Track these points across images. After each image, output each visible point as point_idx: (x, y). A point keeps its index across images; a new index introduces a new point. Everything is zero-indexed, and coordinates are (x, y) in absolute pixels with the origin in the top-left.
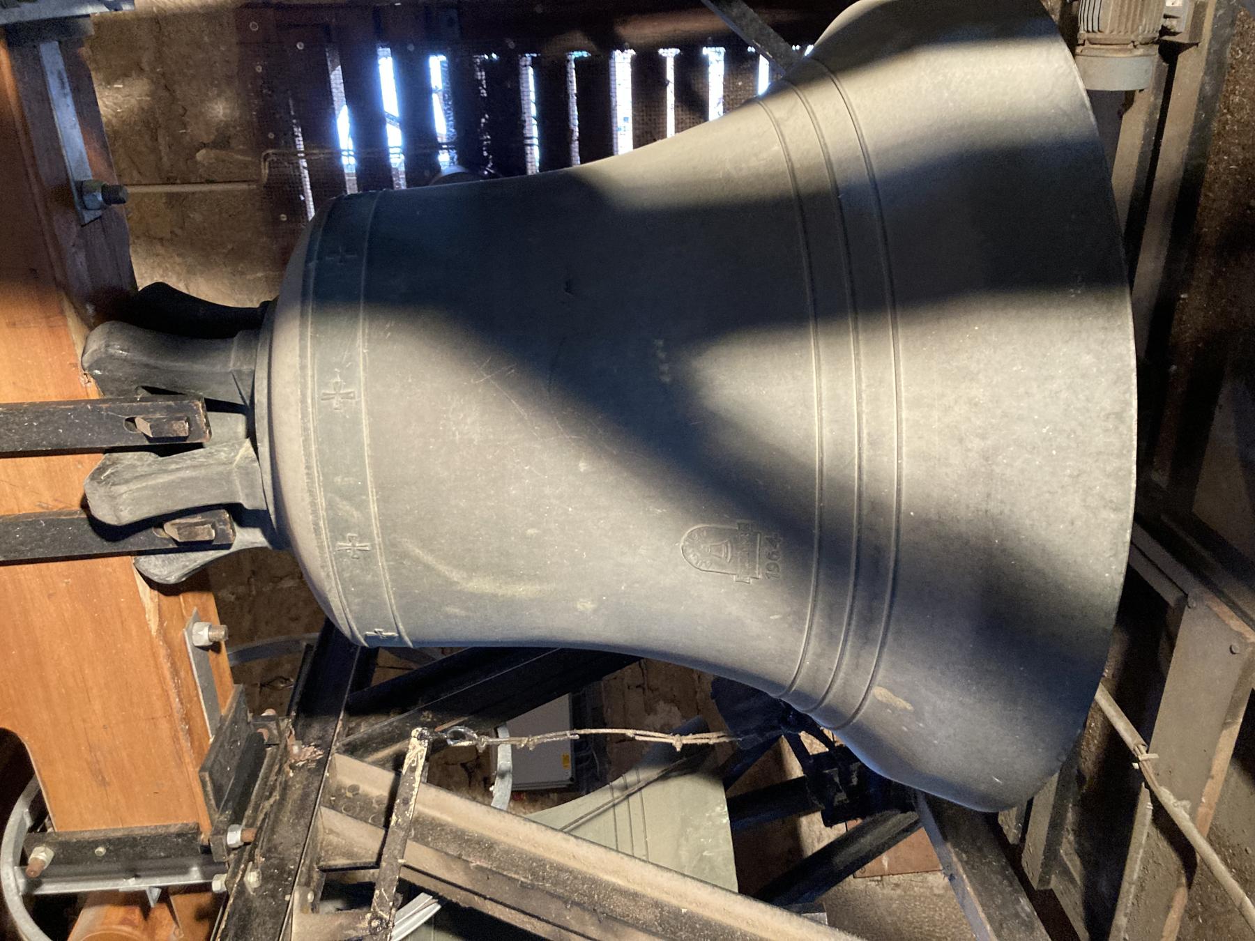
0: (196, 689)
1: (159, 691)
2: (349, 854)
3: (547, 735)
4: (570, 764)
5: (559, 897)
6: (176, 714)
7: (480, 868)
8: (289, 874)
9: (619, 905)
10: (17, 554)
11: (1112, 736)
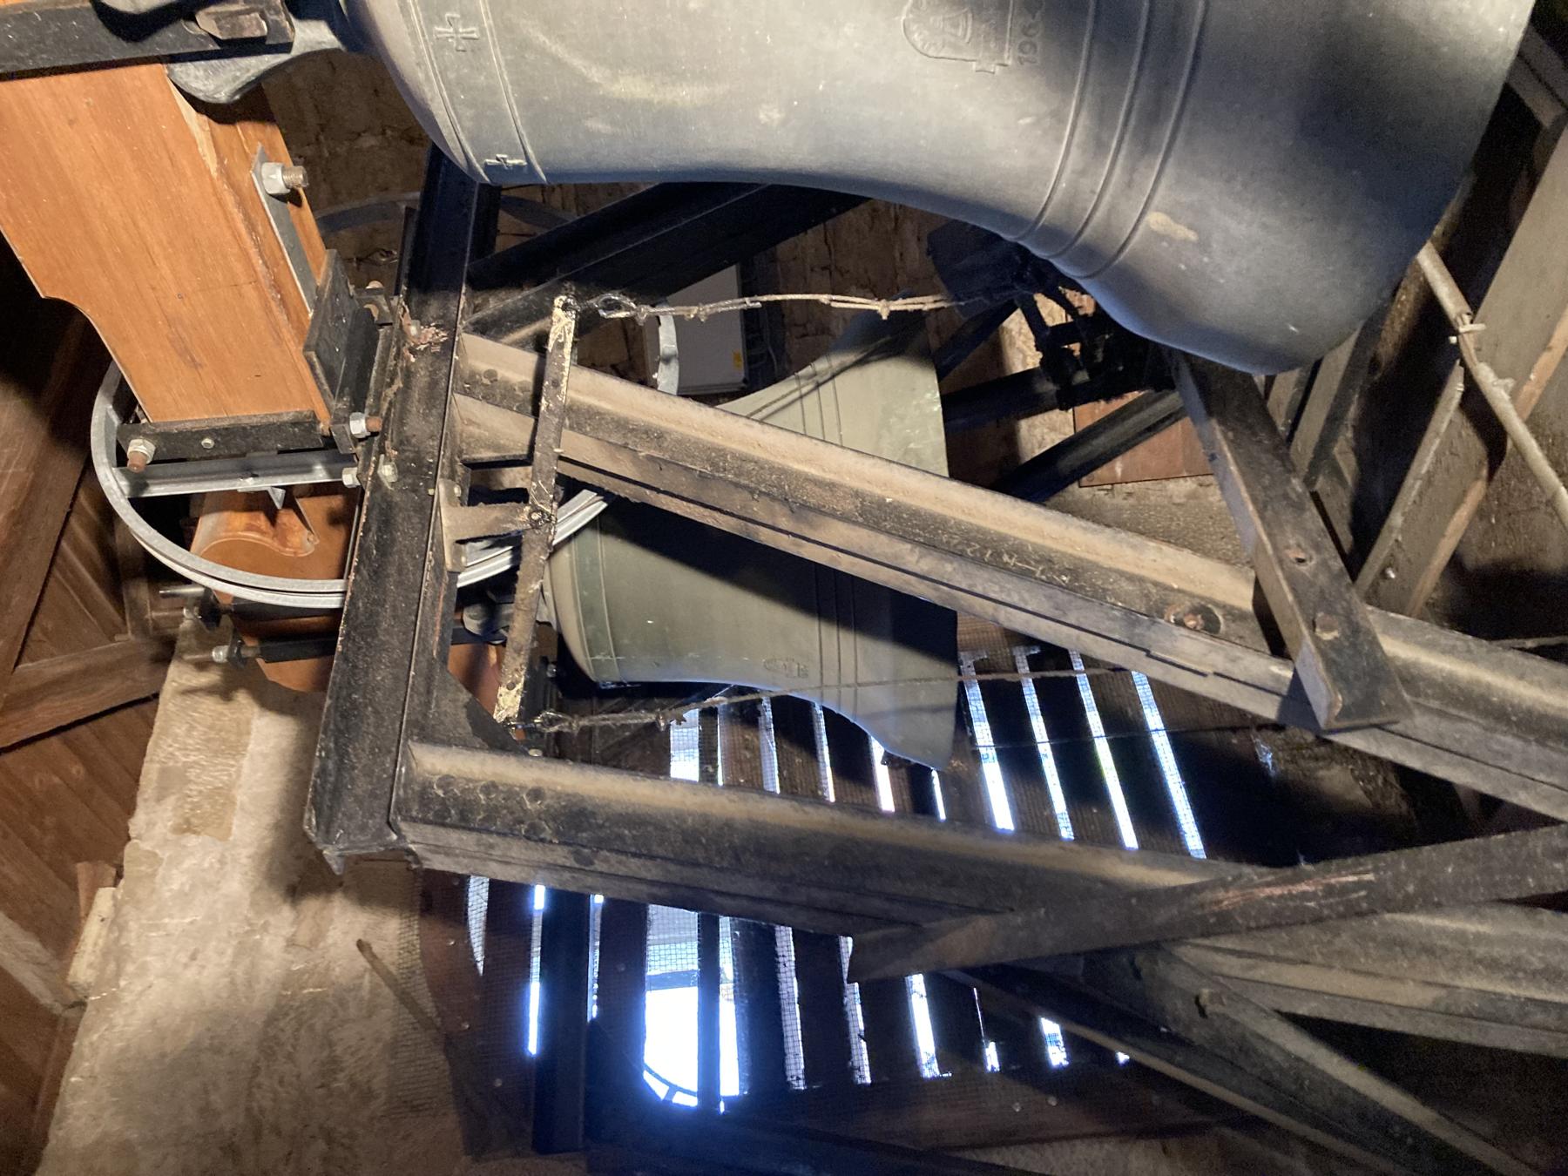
0: (281, 250)
1: (236, 250)
2: (497, 447)
3: (722, 303)
4: (742, 363)
5: (745, 487)
6: (262, 280)
7: (651, 458)
8: (429, 466)
9: (814, 496)
10: (16, 63)
11: (1430, 305)
